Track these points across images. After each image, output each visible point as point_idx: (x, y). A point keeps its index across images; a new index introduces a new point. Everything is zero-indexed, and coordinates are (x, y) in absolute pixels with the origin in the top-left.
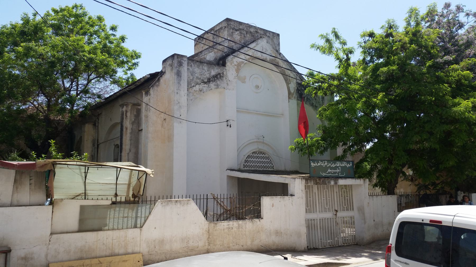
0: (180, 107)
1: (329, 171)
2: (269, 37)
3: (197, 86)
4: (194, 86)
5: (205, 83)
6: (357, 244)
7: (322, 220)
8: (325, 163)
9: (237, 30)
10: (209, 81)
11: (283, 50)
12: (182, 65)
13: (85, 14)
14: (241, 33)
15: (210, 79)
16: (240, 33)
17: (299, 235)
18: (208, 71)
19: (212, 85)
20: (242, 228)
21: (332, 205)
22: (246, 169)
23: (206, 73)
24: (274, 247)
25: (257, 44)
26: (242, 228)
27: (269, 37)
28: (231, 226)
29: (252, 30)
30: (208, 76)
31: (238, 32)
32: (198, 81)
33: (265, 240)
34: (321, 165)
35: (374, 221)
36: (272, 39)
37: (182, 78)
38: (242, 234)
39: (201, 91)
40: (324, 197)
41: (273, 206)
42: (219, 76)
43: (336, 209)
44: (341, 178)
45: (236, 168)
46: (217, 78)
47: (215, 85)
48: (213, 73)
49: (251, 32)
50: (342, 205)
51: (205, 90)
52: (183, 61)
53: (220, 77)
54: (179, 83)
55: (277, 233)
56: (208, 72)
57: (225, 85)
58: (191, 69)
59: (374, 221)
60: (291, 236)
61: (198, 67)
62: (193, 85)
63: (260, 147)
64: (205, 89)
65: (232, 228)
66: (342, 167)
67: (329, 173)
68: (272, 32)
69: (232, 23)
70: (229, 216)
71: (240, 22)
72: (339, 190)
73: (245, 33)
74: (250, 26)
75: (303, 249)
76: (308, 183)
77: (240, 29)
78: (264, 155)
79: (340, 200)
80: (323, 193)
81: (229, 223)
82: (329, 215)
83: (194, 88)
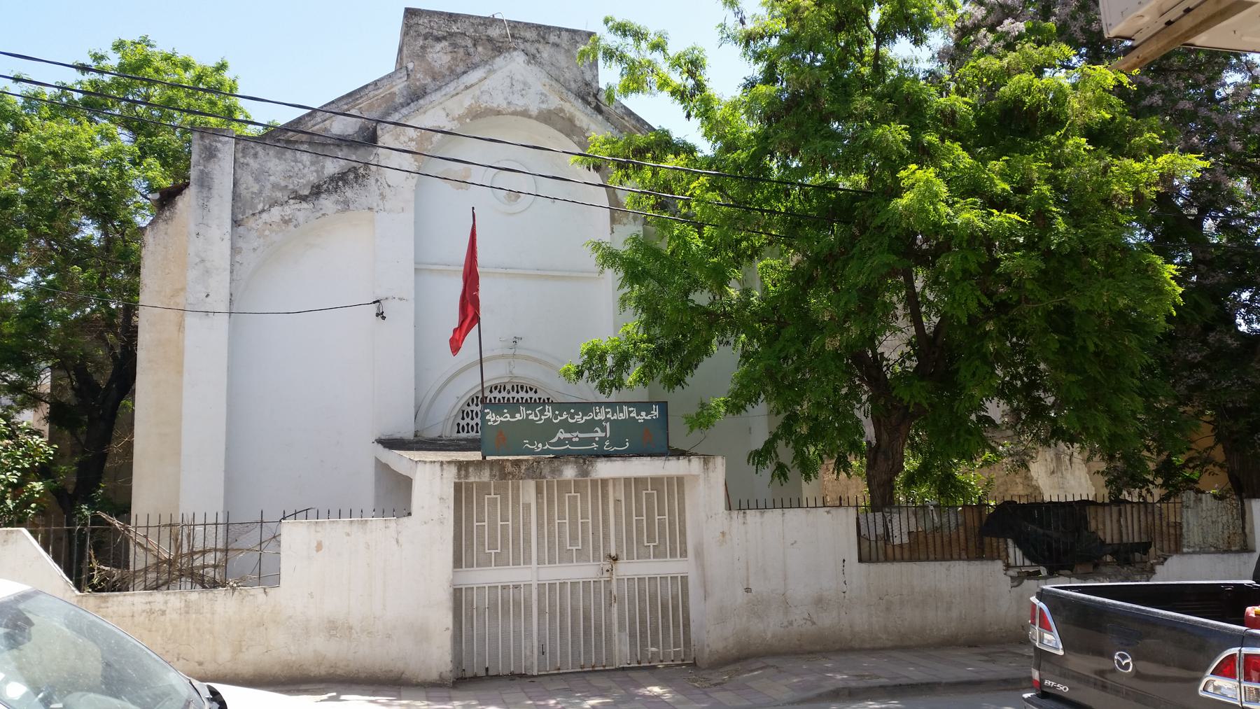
0: (207, 272)
1: (562, 435)
2: (556, 45)
3: (276, 211)
4: (263, 211)
5: (304, 199)
6: (694, 665)
7: (549, 589)
8: (542, 412)
9: (438, 39)
10: (317, 191)
11: (391, 68)
12: (215, 156)
13: (204, 68)
14: (454, 45)
15: (319, 187)
16: (451, 44)
17: (421, 634)
18: (313, 163)
19: (327, 203)
20: (198, 612)
21: (596, 541)
22: (463, 435)
23: (306, 171)
24: (323, 671)
25: (491, 72)
26: (198, 612)
27: (556, 45)
28: (156, 607)
29: (494, 32)
30: (313, 178)
31: (444, 43)
32: (279, 194)
33: (280, 648)
34: (526, 421)
35: (748, 590)
36: (568, 51)
37: (215, 192)
38: (198, 630)
39: (286, 222)
40: (639, 514)
41: (319, 547)
42: (352, 176)
43: (613, 554)
44: (608, 456)
45: (408, 433)
46: (346, 182)
47: (337, 202)
48: (332, 167)
49: (490, 39)
50: (639, 541)
51: (301, 219)
52: (219, 145)
53: (356, 178)
54: (204, 207)
55: (336, 628)
56: (313, 168)
57: (374, 200)
58: (254, 164)
59: (748, 590)
60: (389, 636)
61: (279, 156)
62: (260, 207)
63: (518, 371)
64: (301, 216)
65: (163, 613)
66: (613, 423)
67: (561, 442)
68: (567, 30)
69: (423, 20)
70: (165, 577)
71: (450, 15)
72: (628, 497)
73: (469, 43)
74: (491, 21)
75: (434, 676)
76: (467, 476)
77: (451, 35)
78: (531, 394)
79: (629, 524)
80: (561, 504)
81: (151, 599)
82: (585, 571)
83: (264, 215)
